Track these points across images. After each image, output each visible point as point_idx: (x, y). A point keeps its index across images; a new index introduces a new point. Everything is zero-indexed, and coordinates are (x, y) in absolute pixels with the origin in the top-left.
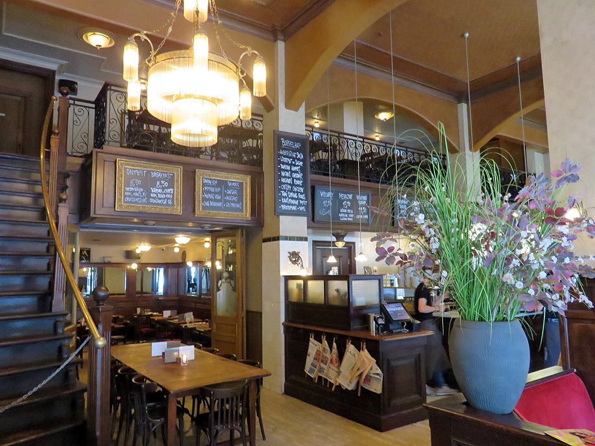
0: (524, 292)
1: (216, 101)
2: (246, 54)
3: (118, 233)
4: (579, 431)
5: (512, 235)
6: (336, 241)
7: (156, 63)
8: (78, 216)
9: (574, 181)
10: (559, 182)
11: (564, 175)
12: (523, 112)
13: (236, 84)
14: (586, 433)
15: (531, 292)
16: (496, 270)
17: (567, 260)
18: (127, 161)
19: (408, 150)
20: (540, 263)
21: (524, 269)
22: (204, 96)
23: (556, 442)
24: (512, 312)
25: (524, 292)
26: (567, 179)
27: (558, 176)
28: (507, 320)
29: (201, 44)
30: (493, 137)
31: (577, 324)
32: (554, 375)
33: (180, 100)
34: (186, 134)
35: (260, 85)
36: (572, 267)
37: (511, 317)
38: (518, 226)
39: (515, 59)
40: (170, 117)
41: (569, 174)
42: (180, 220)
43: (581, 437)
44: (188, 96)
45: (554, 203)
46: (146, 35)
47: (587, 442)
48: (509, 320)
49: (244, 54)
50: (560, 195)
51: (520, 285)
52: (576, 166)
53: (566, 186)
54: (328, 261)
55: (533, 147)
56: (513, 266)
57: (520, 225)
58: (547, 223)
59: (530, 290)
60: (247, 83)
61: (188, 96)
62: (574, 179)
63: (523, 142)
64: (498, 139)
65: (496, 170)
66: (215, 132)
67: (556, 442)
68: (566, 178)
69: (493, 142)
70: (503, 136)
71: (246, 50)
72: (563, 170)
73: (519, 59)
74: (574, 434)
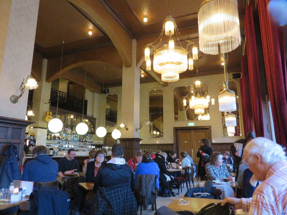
1: (180, 63)
2: (190, 44)
7: (156, 53)
8: (90, 116)
13: (186, 57)
19: (60, 92)
22: (33, 87)
29: (172, 43)
33: (164, 65)
34: (166, 78)
40: (161, 72)
42: (257, 133)
44: (168, 63)
46: (151, 44)
49: (189, 44)
54: (34, 115)
58: (197, 115)
60: (190, 55)
61: (168, 63)
66: (178, 76)
71: (189, 42)
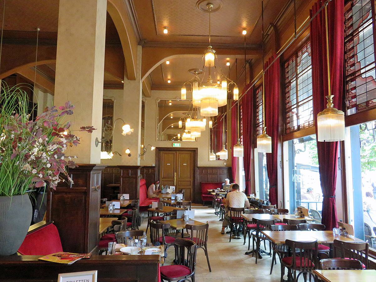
0: (36, 176)
3: (238, 110)
4: (57, 253)
5: (31, 141)
6: (345, 115)
7: (309, 122)
9: (70, 114)
10: (63, 113)
11: (66, 110)
12: (37, 63)
14: (61, 254)
15: (41, 176)
16: (18, 162)
17: (63, 158)
18: (278, 112)
20: (47, 159)
21: (36, 163)
23: (44, 262)
24: (24, 188)
25: (36, 176)
26: (67, 113)
27: (63, 110)
28: (20, 194)
30: (14, 73)
31: (57, 195)
32: (38, 228)
35: (236, 95)
36: (64, 162)
37: (23, 193)
38: (35, 135)
39: (36, 29)
41: (68, 110)
43: (58, 256)
45: (58, 125)
47: (62, 258)
48: (22, 194)
50: (63, 121)
51: (35, 171)
52: (73, 106)
53: (66, 115)
55: (38, 87)
56: (31, 160)
57: (37, 135)
59: (40, 174)
62: (70, 113)
63: (34, 83)
64: (16, 75)
65: (26, 98)
67: (44, 262)
68: (67, 111)
69: (13, 76)
70: (18, 74)
72: (66, 107)
73: (39, 29)
74: (55, 256)
